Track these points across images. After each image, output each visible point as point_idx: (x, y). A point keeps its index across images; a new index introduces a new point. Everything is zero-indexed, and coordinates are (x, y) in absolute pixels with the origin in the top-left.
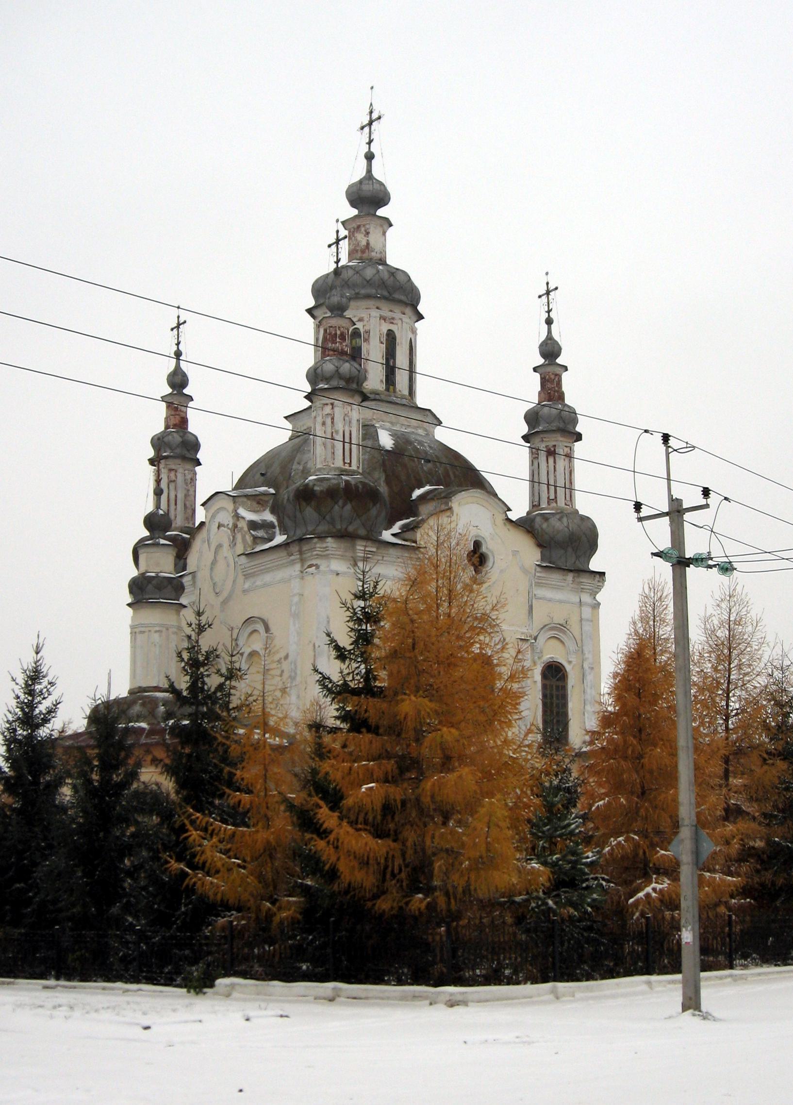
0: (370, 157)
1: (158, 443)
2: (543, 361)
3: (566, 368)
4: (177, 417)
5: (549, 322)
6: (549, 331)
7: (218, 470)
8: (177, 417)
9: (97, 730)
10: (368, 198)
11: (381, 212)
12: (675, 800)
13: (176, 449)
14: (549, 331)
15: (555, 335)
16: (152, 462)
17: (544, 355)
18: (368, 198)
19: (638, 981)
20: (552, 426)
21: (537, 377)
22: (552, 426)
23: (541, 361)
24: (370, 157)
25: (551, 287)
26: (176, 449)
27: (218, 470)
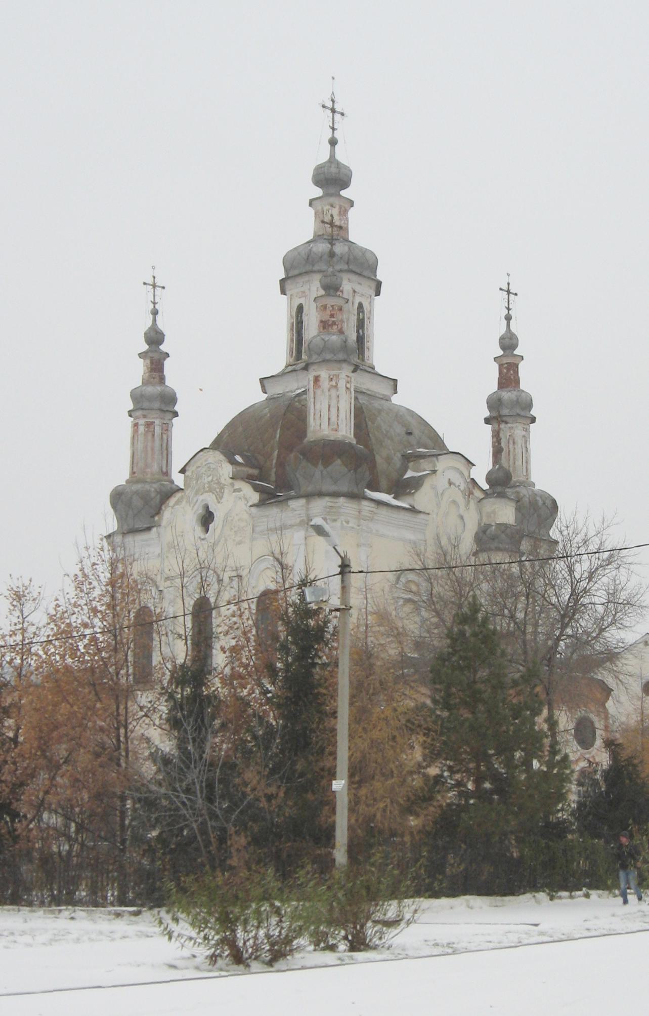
0: (333, 142)
1: (138, 397)
2: (147, 347)
3: (167, 355)
4: (509, 375)
5: (508, 318)
6: (155, 320)
7: (195, 430)
8: (509, 375)
9: (285, 727)
10: (332, 180)
11: (343, 193)
12: (333, 730)
13: (155, 404)
14: (155, 320)
15: (160, 325)
16: (487, 421)
17: (503, 347)
18: (332, 180)
19: (444, 901)
20: (509, 410)
21: (496, 367)
22: (509, 410)
23: (146, 347)
24: (333, 142)
25: (150, 281)
26: (155, 404)
27: (195, 430)
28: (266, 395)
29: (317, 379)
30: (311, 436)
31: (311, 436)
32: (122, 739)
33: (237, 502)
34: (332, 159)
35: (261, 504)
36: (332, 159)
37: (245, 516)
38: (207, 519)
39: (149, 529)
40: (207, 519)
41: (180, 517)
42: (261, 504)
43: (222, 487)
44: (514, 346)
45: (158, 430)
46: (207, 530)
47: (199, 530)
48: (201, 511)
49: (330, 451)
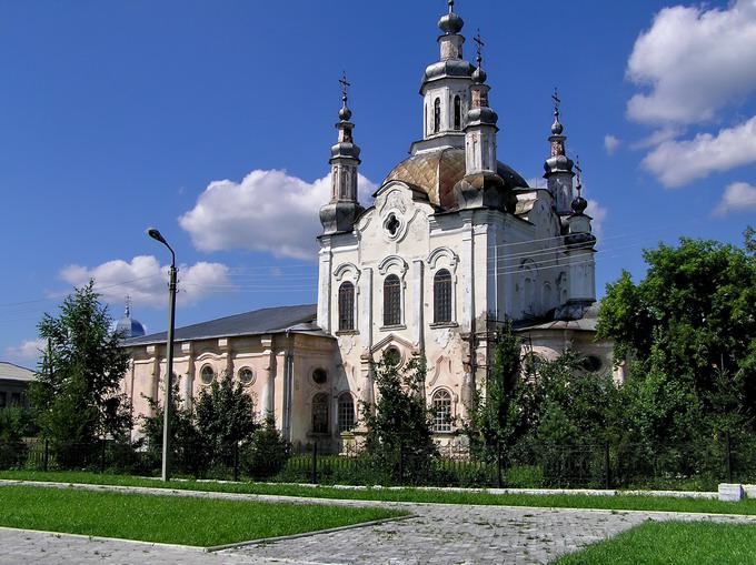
38: (392, 224)
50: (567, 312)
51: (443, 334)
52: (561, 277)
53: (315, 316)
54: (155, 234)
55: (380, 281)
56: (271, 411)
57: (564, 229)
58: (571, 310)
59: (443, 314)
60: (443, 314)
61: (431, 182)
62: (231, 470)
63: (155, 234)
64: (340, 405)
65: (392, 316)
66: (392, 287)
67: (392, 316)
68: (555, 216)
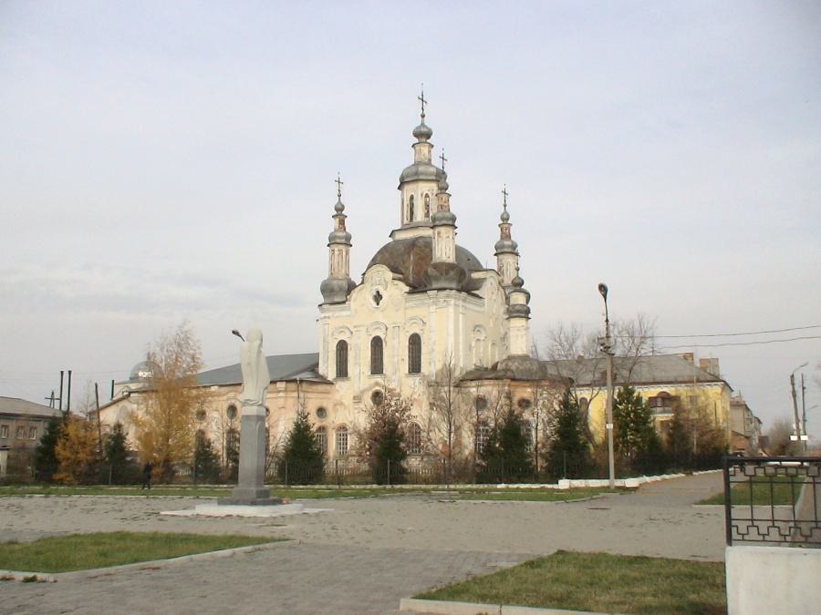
0: (423, 116)
4: (506, 235)
13: (341, 240)
20: (506, 248)
23: (335, 213)
24: (423, 116)
26: (341, 240)
28: (391, 240)
29: (439, 233)
30: (434, 261)
31: (434, 261)
32: (783, 463)
33: (395, 291)
34: (423, 124)
35: (409, 293)
36: (423, 124)
37: (400, 297)
38: (378, 297)
39: (344, 302)
40: (378, 297)
41: (361, 298)
42: (409, 293)
43: (386, 283)
44: (342, 210)
45: (344, 253)
46: (378, 304)
47: (374, 304)
48: (375, 293)
49: (445, 269)
50: (506, 365)
51: (416, 379)
52: (505, 338)
53: (317, 365)
54: (603, 289)
55: (333, 347)
56: (457, 350)
57: (507, 298)
58: (510, 364)
59: (415, 367)
60: (415, 367)
61: (407, 265)
62: (273, 471)
63: (603, 289)
64: (337, 434)
65: (377, 367)
66: (377, 344)
67: (377, 367)
68: (501, 289)
